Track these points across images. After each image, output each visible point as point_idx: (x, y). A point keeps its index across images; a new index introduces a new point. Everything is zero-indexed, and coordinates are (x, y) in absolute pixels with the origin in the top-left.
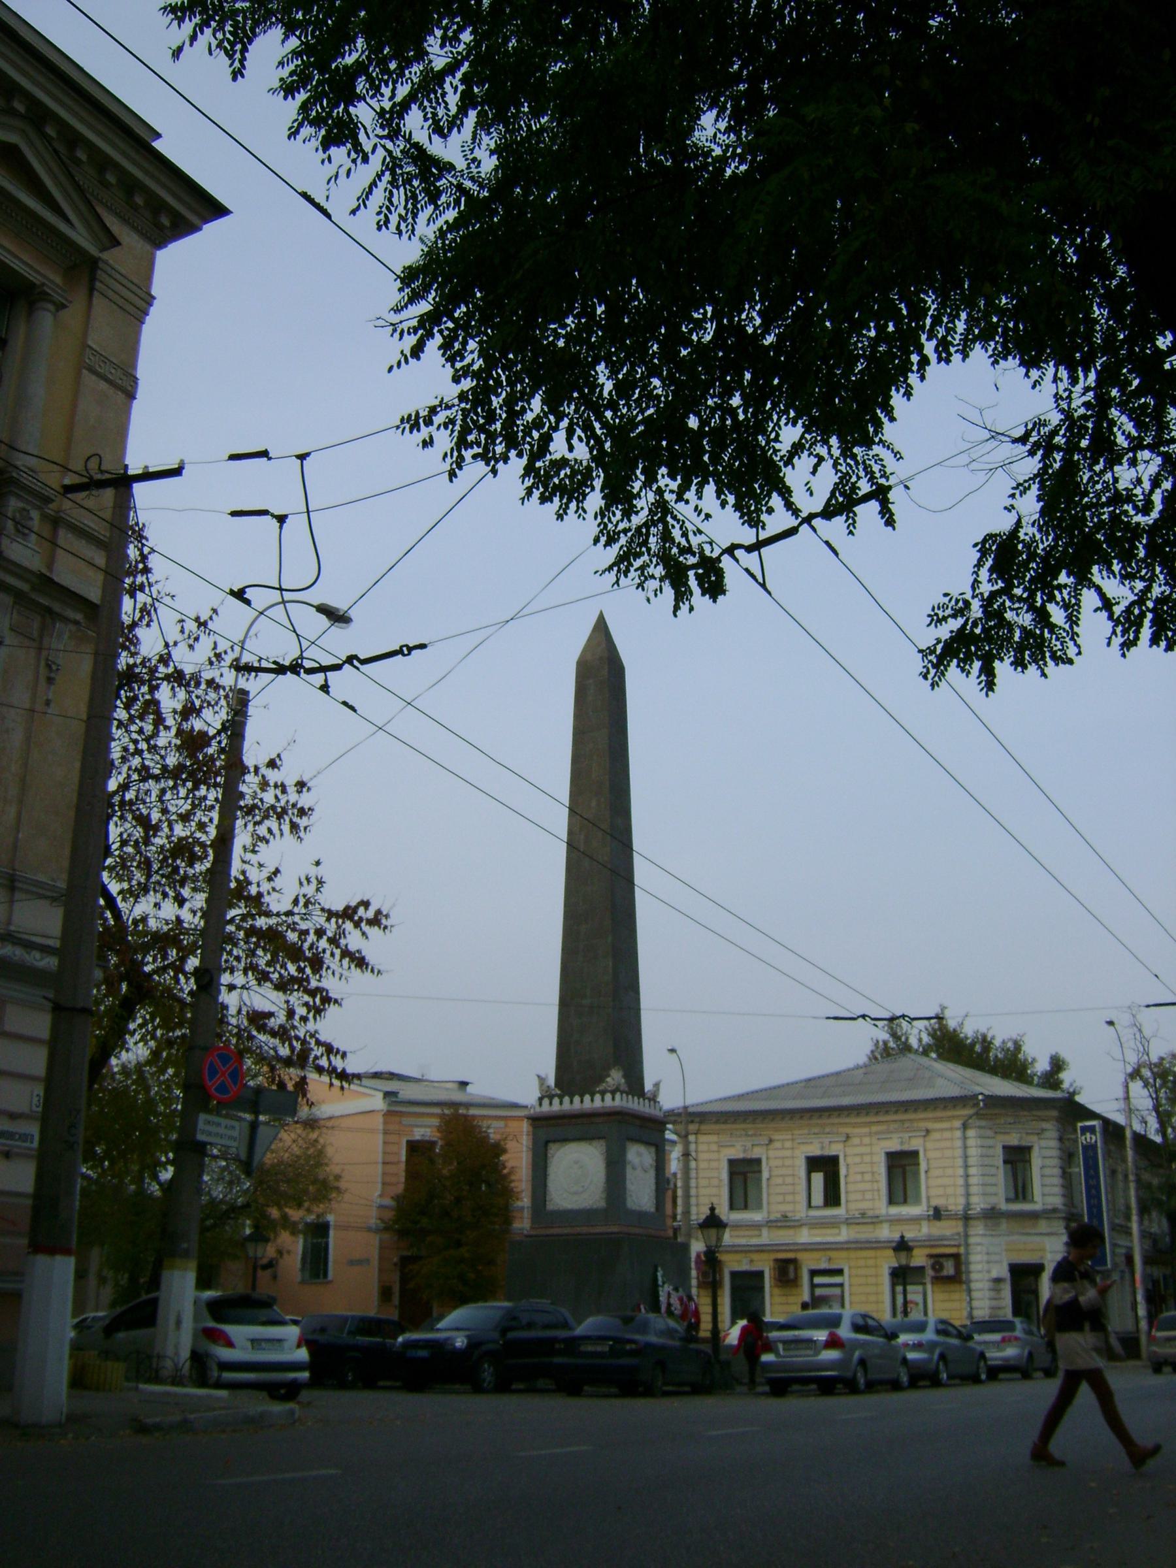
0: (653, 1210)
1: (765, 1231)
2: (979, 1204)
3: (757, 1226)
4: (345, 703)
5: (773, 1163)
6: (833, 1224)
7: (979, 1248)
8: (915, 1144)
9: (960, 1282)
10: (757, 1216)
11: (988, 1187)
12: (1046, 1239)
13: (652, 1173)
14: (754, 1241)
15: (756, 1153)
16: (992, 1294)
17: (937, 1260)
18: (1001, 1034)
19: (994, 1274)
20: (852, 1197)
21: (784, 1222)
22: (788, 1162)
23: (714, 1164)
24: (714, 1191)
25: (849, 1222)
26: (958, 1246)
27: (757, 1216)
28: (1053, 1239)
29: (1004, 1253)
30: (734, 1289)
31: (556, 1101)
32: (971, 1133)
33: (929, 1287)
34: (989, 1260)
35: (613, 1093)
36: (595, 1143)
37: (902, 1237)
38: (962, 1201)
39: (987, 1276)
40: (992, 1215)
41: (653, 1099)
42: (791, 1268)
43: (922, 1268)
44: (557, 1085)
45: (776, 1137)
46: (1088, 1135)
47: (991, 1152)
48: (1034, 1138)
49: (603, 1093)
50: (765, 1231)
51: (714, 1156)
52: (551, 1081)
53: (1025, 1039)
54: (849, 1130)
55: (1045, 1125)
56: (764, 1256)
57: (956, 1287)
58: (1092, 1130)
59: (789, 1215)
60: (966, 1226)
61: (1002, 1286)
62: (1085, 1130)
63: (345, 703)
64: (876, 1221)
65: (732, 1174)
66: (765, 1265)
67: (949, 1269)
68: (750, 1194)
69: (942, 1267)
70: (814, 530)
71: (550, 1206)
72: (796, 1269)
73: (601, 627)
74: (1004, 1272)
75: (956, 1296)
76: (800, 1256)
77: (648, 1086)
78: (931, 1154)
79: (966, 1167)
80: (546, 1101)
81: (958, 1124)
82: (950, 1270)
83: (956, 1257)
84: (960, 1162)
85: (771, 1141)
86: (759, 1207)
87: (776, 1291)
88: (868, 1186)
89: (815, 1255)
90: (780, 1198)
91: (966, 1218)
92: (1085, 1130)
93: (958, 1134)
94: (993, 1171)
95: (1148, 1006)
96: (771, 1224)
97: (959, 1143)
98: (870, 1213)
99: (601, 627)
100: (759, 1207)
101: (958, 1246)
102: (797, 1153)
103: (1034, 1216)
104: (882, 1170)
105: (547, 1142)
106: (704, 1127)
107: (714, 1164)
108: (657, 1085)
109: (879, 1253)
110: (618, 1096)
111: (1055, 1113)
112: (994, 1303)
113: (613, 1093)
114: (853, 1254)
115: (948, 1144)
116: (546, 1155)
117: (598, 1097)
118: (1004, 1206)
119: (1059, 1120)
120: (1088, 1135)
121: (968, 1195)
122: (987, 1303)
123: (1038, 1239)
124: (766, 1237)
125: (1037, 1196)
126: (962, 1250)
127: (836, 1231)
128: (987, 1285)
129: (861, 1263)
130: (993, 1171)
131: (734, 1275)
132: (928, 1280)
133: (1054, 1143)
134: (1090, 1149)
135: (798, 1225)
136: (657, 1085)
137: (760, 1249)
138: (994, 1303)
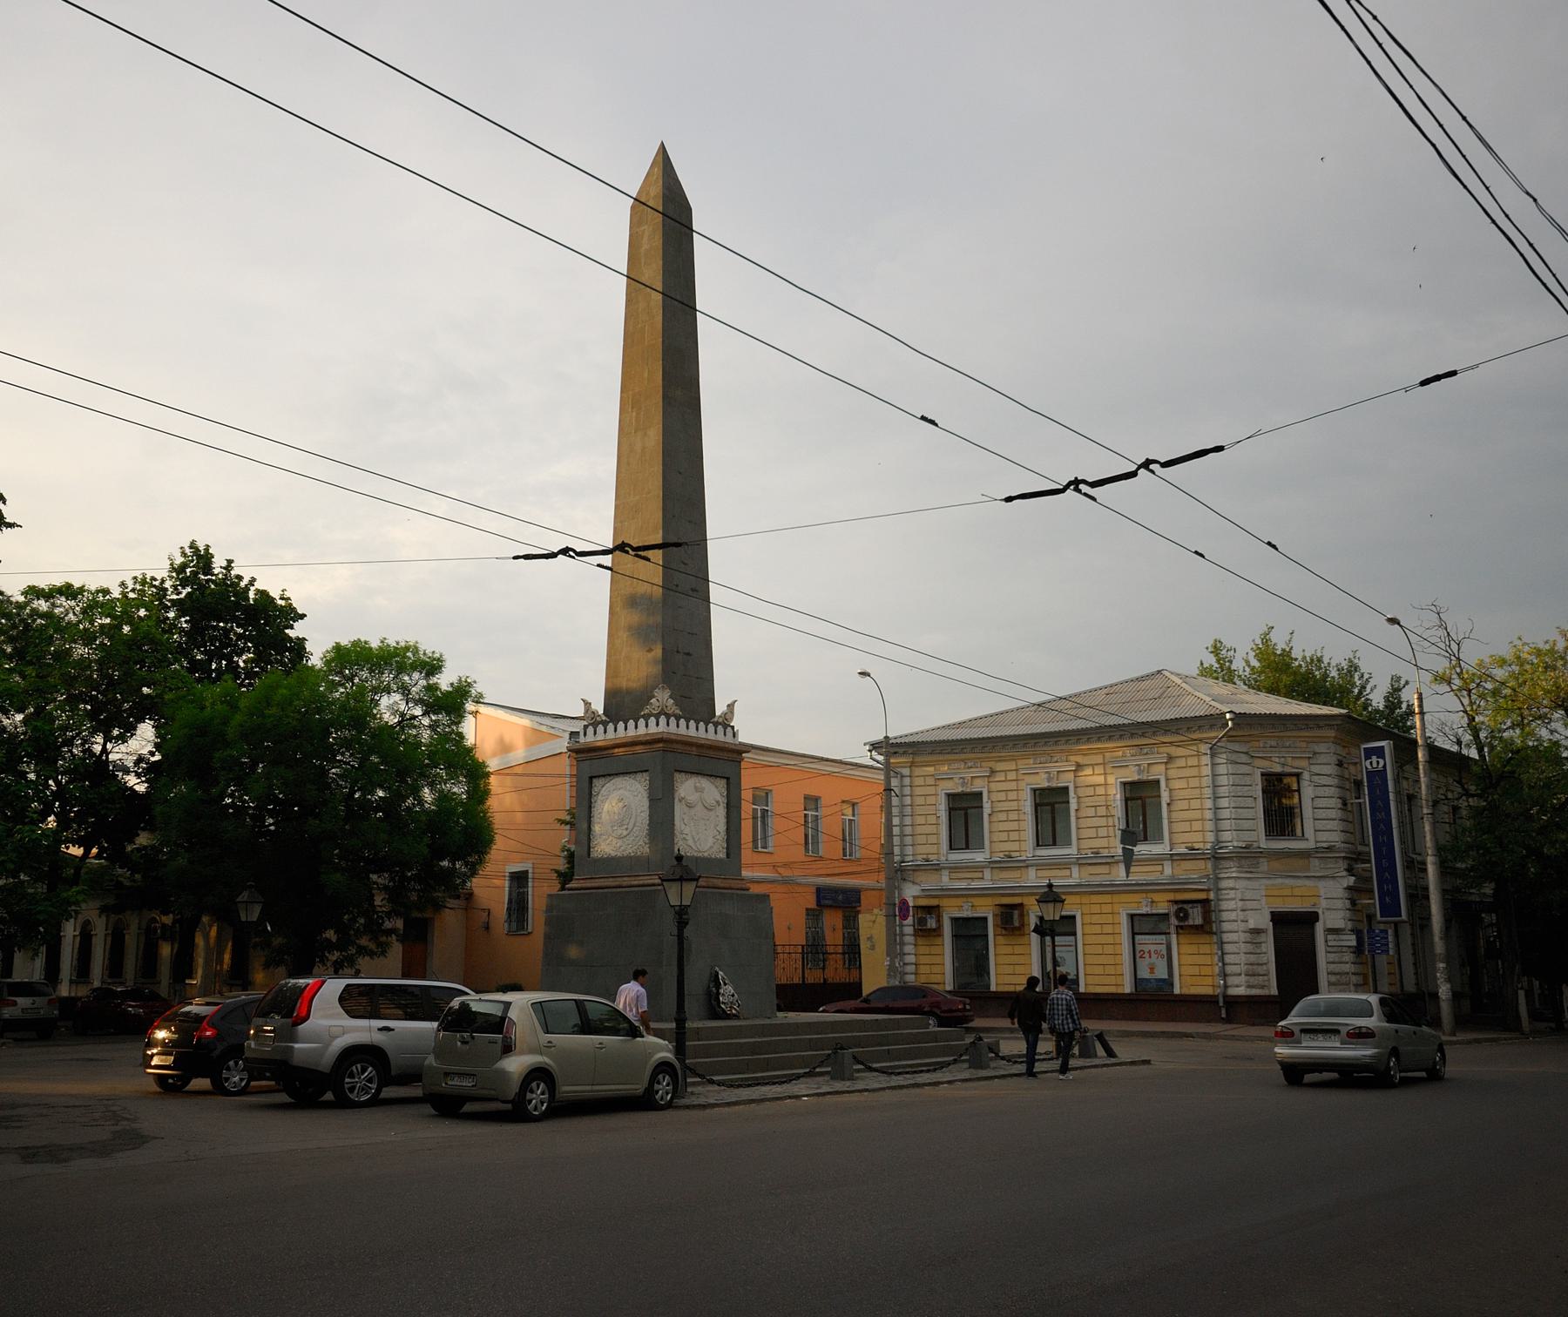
0: (722, 855)
1: (987, 874)
2: (1231, 840)
3: (978, 868)
4: (1269, 543)
5: (995, 797)
6: (1063, 864)
7: (1232, 894)
8: (1157, 772)
9: (1211, 933)
10: (979, 857)
11: (1246, 823)
12: (1321, 884)
13: (722, 811)
14: (975, 884)
15: (978, 786)
16: (1250, 947)
17: (1182, 909)
18: (1335, 657)
19: (1252, 924)
20: (1178, 827)
21: (1008, 863)
22: (1012, 796)
23: (931, 800)
24: (932, 829)
25: (1081, 862)
26: (1208, 890)
27: (979, 857)
28: (1330, 883)
29: (1264, 900)
30: (955, 936)
31: (600, 728)
32: (1222, 759)
33: (1174, 937)
34: (1246, 907)
35: (657, 717)
36: (639, 776)
37: (1050, 886)
38: (1210, 837)
39: (1242, 926)
40: (1248, 856)
41: (725, 723)
42: (1016, 913)
43: (1167, 915)
44: (605, 713)
45: (1000, 766)
46: (1374, 759)
47: (1248, 780)
48: (1304, 763)
49: (647, 718)
50: (987, 874)
51: (931, 790)
52: (599, 706)
53: (1279, 641)
54: (1080, 759)
55: (1322, 748)
56: (989, 901)
57: (1206, 938)
58: (1380, 752)
59: (931, 857)
60: (1215, 868)
61: (1262, 938)
62: (1369, 753)
63: (1269, 543)
64: (1025, 865)
65: (951, 810)
66: (986, 909)
67: (1196, 918)
68: (1058, 827)
69: (1186, 917)
70: (1152, 472)
71: (595, 854)
72: (1022, 915)
73: (663, 162)
74: (1265, 922)
75: (1205, 949)
76: (944, 902)
77: (720, 709)
78: (1176, 784)
79: (1216, 798)
80: (590, 730)
81: (1204, 748)
82: (1195, 916)
83: (1205, 903)
84: (1208, 792)
85: (993, 772)
86: (981, 846)
87: (1001, 940)
88: (1103, 822)
89: (959, 902)
90: (1004, 836)
91: (1216, 857)
92: (1369, 753)
93: (1206, 760)
94: (1250, 802)
95: (1009, 499)
96: (993, 865)
97: (1207, 771)
98: (1105, 853)
99: (663, 162)
100: (981, 846)
101: (1208, 890)
102: (1022, 785)
103: (1305, 855)
104: (1028, 807)
105: (591, 778)
106: (918, 759)
107: (931, 800)
108: (731, 706)
109: (1116, 898)
110: (663, 719)
111: (1332, 733)
112: (1252, 958)
113: (657, 717)
114: (1085, 899)
115: (1194, 772)
116: (590, 794)
117: (642, 722)
118: (1264, 844)
119: (1337, 741)
120: (1374, 759)
121: (1218, 831)
122: (1243, 958)
123: (1307, 882)
124: (988, 880)
125: (1309, 832)
126: (1212, 896)
127: (1067, 872)
128: (1243, 937)
129: (1096, 909)
130: (1250, 802)
131: (955, 920)
132: (1172, 929)
133: (1331, 769)
134: (1377, 777)
135: (1025, 865)
136: (731, 706)
137: (983, 893)
138: (1252, 958)
